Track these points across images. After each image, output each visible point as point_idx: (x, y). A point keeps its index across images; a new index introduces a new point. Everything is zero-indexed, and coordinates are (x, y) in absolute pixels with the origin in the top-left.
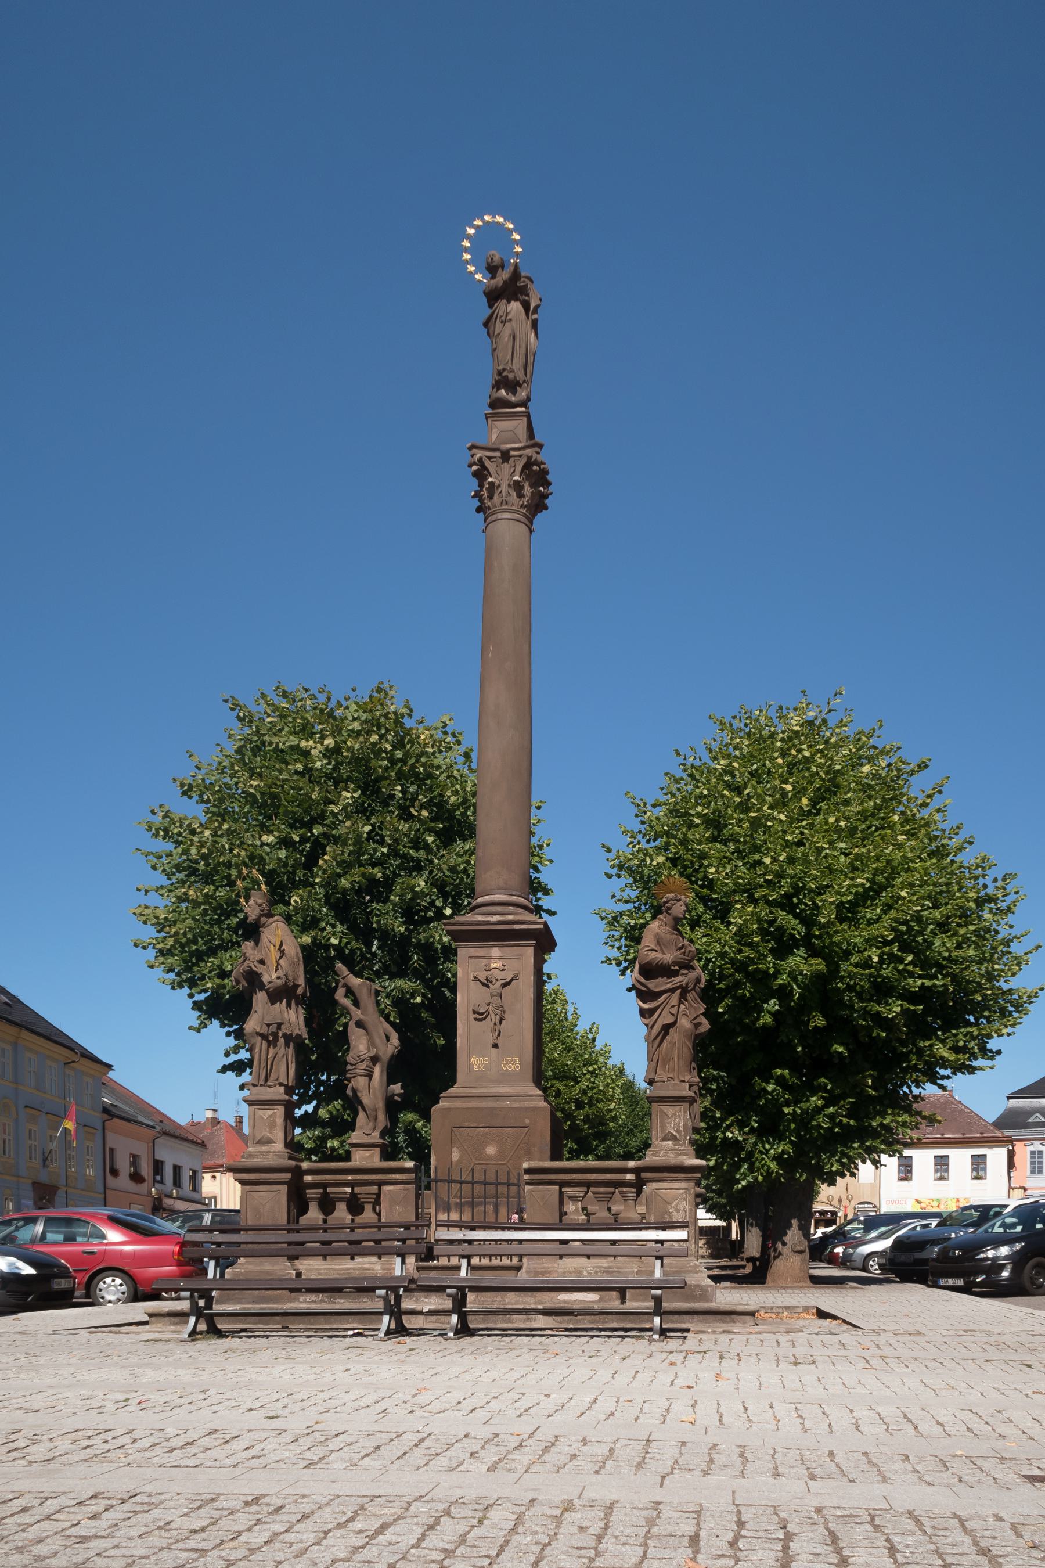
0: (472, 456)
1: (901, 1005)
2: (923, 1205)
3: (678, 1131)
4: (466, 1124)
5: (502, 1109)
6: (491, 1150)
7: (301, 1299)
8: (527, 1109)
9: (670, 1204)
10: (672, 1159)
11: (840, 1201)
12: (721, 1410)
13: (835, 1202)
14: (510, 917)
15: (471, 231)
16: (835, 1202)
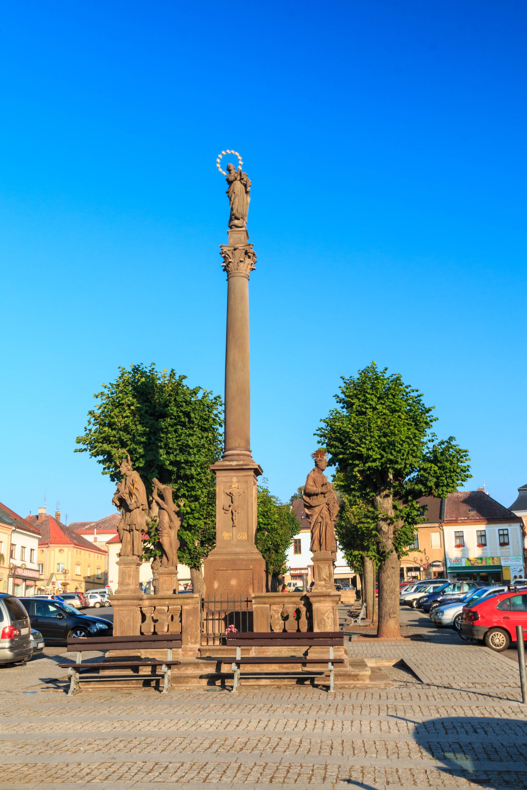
0: (222, 250)
1: (435, 490)
2: (473, 562)
3: (327, 576)
4: (221, 569)
5: (239, 559)
6: (233, 582)
7: (144, 670)
8: (251, 560)
9: (324, 614)
10: (324, 590)
11: (421, 561)
12: (354, 745)
13: (419, 561)
14: (241, 463)
15: (220, 156)
16: (419, 561)
